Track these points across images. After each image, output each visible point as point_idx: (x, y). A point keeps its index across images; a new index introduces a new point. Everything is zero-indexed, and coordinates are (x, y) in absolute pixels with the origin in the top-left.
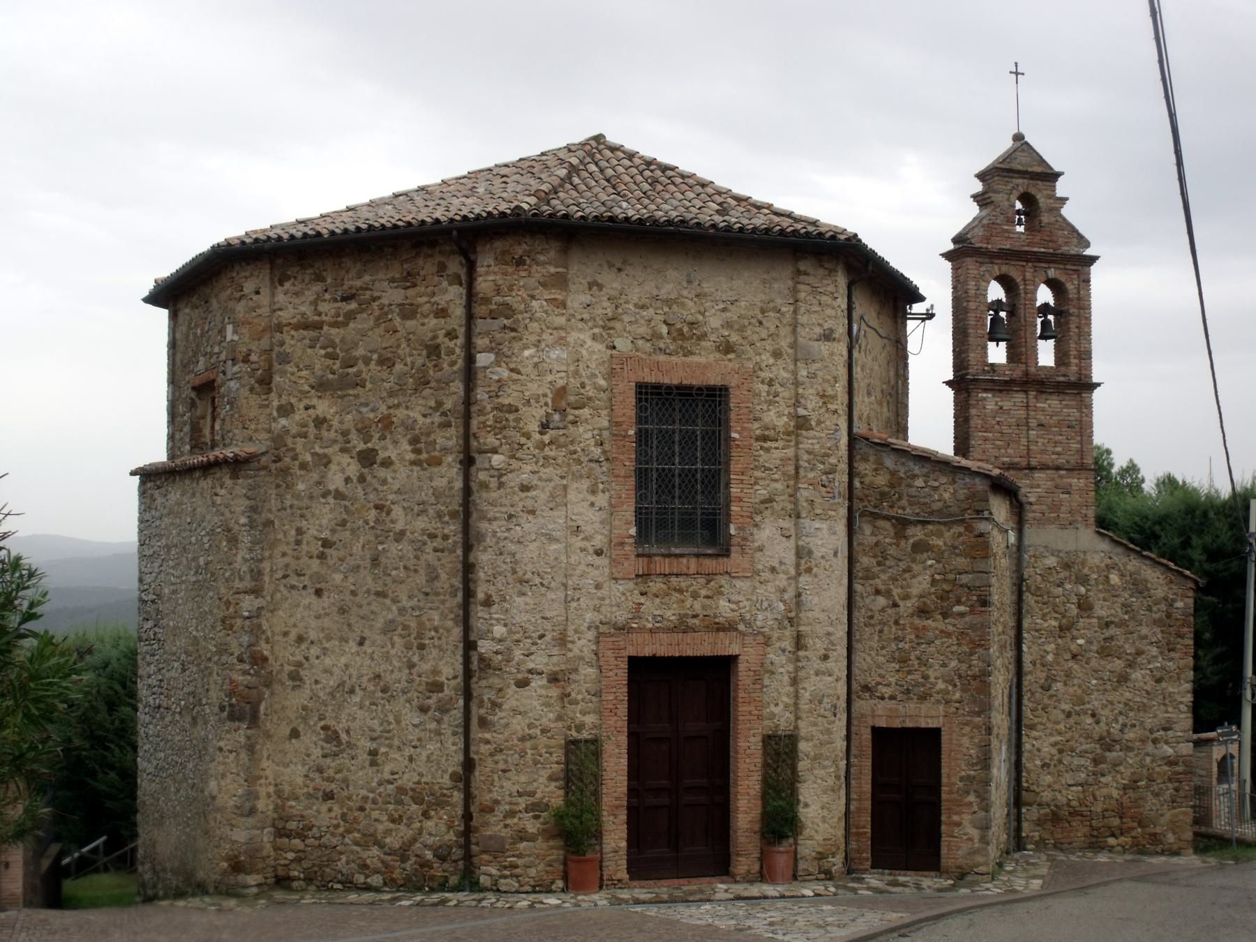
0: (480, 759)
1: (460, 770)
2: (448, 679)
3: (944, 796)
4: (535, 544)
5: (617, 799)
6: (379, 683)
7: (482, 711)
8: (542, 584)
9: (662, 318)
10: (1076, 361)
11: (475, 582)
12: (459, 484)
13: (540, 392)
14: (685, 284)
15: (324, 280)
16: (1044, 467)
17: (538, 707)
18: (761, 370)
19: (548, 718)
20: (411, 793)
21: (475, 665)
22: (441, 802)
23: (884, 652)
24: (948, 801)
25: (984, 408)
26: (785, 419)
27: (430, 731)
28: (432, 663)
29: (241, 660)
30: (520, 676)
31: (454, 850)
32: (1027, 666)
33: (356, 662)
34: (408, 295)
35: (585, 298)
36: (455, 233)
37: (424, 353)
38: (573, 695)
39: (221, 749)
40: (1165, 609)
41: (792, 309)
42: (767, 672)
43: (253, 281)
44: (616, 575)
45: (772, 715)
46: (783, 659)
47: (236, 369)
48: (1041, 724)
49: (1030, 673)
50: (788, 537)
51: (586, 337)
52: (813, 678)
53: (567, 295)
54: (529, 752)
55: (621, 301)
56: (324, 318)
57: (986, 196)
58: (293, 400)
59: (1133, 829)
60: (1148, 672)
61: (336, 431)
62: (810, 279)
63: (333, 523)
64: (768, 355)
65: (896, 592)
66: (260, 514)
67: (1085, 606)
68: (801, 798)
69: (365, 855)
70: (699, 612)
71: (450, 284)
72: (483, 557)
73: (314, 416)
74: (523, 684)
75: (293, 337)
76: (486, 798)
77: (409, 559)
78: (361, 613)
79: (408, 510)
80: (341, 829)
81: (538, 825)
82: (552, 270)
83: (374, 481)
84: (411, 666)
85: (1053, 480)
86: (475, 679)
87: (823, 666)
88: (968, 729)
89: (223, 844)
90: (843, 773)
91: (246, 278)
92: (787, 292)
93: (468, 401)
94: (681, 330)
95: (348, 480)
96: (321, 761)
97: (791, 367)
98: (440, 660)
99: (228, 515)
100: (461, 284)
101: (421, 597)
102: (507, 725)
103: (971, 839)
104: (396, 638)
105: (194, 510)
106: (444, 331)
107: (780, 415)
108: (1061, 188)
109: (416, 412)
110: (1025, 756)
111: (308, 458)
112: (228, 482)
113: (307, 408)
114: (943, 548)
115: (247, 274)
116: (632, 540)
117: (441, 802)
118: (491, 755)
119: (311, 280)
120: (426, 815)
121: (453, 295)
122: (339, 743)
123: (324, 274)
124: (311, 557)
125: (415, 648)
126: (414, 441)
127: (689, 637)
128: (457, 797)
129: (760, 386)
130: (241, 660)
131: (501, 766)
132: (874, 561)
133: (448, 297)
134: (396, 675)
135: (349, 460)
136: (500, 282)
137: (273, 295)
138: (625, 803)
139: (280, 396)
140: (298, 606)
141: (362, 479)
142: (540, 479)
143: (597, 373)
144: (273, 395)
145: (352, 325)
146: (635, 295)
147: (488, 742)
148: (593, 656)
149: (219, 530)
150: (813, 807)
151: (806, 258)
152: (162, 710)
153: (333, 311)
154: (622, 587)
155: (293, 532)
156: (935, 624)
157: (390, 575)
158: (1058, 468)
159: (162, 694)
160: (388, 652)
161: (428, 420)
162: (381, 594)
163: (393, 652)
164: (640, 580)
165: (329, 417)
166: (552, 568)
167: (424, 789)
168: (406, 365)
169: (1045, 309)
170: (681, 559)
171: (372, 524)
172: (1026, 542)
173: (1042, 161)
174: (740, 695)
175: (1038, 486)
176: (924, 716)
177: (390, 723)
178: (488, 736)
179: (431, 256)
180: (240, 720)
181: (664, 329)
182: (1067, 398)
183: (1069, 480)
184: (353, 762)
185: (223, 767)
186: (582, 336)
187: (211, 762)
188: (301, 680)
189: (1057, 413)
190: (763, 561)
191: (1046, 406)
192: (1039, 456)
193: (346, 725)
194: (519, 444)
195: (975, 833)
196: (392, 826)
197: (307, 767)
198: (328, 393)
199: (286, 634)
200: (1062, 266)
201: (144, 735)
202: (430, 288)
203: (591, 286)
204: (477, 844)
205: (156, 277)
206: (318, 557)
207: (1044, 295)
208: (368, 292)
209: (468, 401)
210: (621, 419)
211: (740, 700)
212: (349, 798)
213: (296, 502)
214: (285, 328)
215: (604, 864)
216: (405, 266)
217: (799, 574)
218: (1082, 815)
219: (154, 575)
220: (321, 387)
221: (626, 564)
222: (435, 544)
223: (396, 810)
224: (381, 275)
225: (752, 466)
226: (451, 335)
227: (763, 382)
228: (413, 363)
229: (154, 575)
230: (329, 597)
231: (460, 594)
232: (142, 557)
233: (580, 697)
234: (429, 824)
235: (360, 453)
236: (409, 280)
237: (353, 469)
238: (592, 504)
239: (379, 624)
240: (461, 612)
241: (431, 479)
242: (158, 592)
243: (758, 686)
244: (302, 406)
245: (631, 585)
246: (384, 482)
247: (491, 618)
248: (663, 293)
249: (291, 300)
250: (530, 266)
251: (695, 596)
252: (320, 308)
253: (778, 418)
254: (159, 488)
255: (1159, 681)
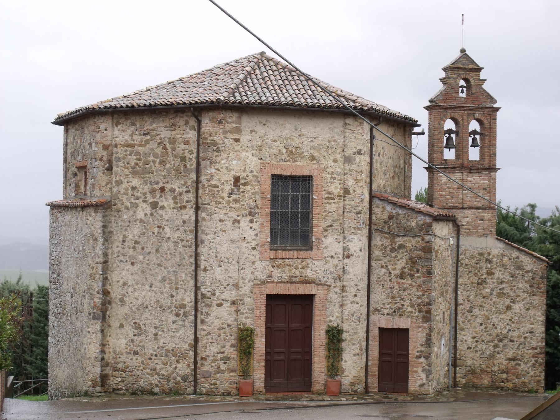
0: (201, 337)
1: (193, 342)
2: (188, 303)
3: (410, 359)
4: (226, 245)
5: (261, 356)
6: (158, 304)
7: (202, 317)
8: (228, 262)
9: (283, 145)
10: (488, 158)
11: (200, 261)
12: (193, 218)
13: (228, 179)
14: (294, 130)
15: (135, 125)
16: (470, 208)
17: (226, 315)
18: (328, 168)
19: (230, 320)
20: (171, 352)
21: (199, 297)
22: (184, 356)
23: (384, 294)
24: (413, 361)
25: (441, 181)
26: (339, 190)
27: (180, 325)
28: (182, 295)
29: (98, 293)
30: (219, 302)
31: (190, 377)
32: (460, 300)
33: (148, 295)
34: (172, 134)
35: (249, 137)
36: (192, 109)
37: (179, 160)
38: (242, 310)
39: (89, 332)
40: (531, 275)
41: (343, 141)
42: (328, 302)
43: (104, 124)
44: (261, 259)
45: (331, 321)
46: (336, 296)
47: (97, 163)
48: (467, 328)
49: (462, 304)
50: (339, 242)
51: (249, 154)
52: (349, 305)
53: (241, 136)
54: (222, 335)
55: (265, 138)
56: (136, 142)
57: (445, 80)
58: (122, 179)
59: (514, 379)
60: (522, 305)
61: (141, 193)
62: (351, 127)
63: (139, 233)
64: (331, 161)
65: (390, 267)
66: (107, 228)
67: (490, 273)
68: (343, 358)
69: (151, 379)
70: (298, 275)
71: (190, 130)
72: (202, 250)
73: (131, 186)
74: (220, 305)
75: (122, 150)
76: (204, 355)
77: (172, 250)
78: (151, 272)
79: (172, 229)
80: (141, 368)
81: (226, 366)
82: (234, 125)
83: (157, 215)
84: (172, 296)
85: (475, 214)
86: (199, 303)
87: (354, 299)
88: (420, 329)
89: (89, 374)
90: (364, 348)
91: (101, 123)
92: (340, 133)
93: (198, 182)
94: (292, 151)
95: (146, 215)
96: (133, 337)
97: (342, 167)
98: (185, 294)
99: (93, 228)
100: (195, 130)
101: (177, 266)
102: (212, 323)
103: (422, 379)
104: (165, 284)
105: (77, 225)
106: (188, 150)
107: (336, 188)
108: (483, 75)
109: (176, 185)
110: (459, 343)
111: (129, 204)
112: (93, 214)
113: (128, 182)
114: (412, 247)
115: (102, 121)
116: (269, 243)
117: (184, 356)
118: (206, 335)
119: (130, 125)
120: (178, 362)
121: (192, 135)
122: (141, 330)
123: (136, 122)
124: (129, 248)
125: (174, 289)
126: (175, 198)
127: (293, 286)
128: (192, 353)
129: (327, 175)
130: (98, 293)
131: (210, 340)
132: (381, 253)
133: (189, 136)
134: (166, 300)
135: (147, 206)
136: (212, 131)
137: (113, 131)
138: (264, 358)
139: (116, 176)
140: (123, 270)
141: (152, 214)
142: (228, 217)
143: (254, 170)
144: (113, 176)
145: (148, 146)
146: (272, 135)
147: (204, 330)
148: (250, 293)
149: (89, 235)
150: (349, 362)
151: (349, 118)
152: (61, 314)
153: (139, 139)
154: (264, 263)
155: (122, 237)
156: (407, 281)
157: (164, 257)
158: (477, 208)
159: (61, 307)
160: (162, 290)
161: (181, 190)
162: (159, 265)
163: (164, 290)
164: (272, 261)
165: (138, 186)
166: (233, 255)
167: (177, 350)
168: (171, 165)
169: (474, 132)
170: (290, 252)
171: (156, 234)
172: (460, 244)
173: (473, 62)
174: (316, 312)
175: (467, 217)
176: (401, 323)
177: (163, 321)
178: (205, 327)
179: (183, 117)
180: (97, 319)
181: (284, 151)
182: (483, 175)
183: (483, 214)
184: (147, 338)
185: (90, 340)
186: (247, 154)
187: (84, 338)
188: (125, 302)
189: (477, 183)
190: (327, 253)
191: (472, 179)
192: (468, 203)
193: (144, 322)
194: (219, 202)
195: (423, 376)
196: (163, 366)
197: (127, 340)
198: (137, 176)
199: (118, 282)
200: (482, 113)
201: (52, 326)
202: (182, 131)
203: (252, 132)
204: (199, 374)
205: (59, 113)
206: (133, 248)
207: (474, 125)
208: (155, 132)
209: (198, 182)
210: (264, 191)
211: (316, 314)
212: (145, 354)
213: (123, 224)
214: (118, 146)
215: (254, 384)
216: (171, 121)
217: (344, 259)
218: (487, 372)
219: (57, 252)
220: (134, 173)
221: (265, 254)
222: (183, 244)
223: (165, 360)
224: (161, 124)
225: (323, 211)
226: (191, 152)
227: (328, 174)
228: (174, 164)
229: (57, 252)
230: (137, 266)
231: (194, 266)
232: (51, 244)
233: (244, 311)
234: (179, 366)
235: (151, 203)
236: (173, 127)
237: (148, 210)
238: (251, 228)
239: (159, 278)
240: (194, 274)
241: (182, 215)
242: (60, 261)
243: (324, 308)
244: (126, 181)
245: (268, 263)
246: (161, 216)
247: (206, 276)
248: (284, 135)
249: (121, 133)
250: (224, 124)
251: (296, 268)
252: (134, 138)
253: (336, 188)
254: (60, 213)
255: (528, 309)
